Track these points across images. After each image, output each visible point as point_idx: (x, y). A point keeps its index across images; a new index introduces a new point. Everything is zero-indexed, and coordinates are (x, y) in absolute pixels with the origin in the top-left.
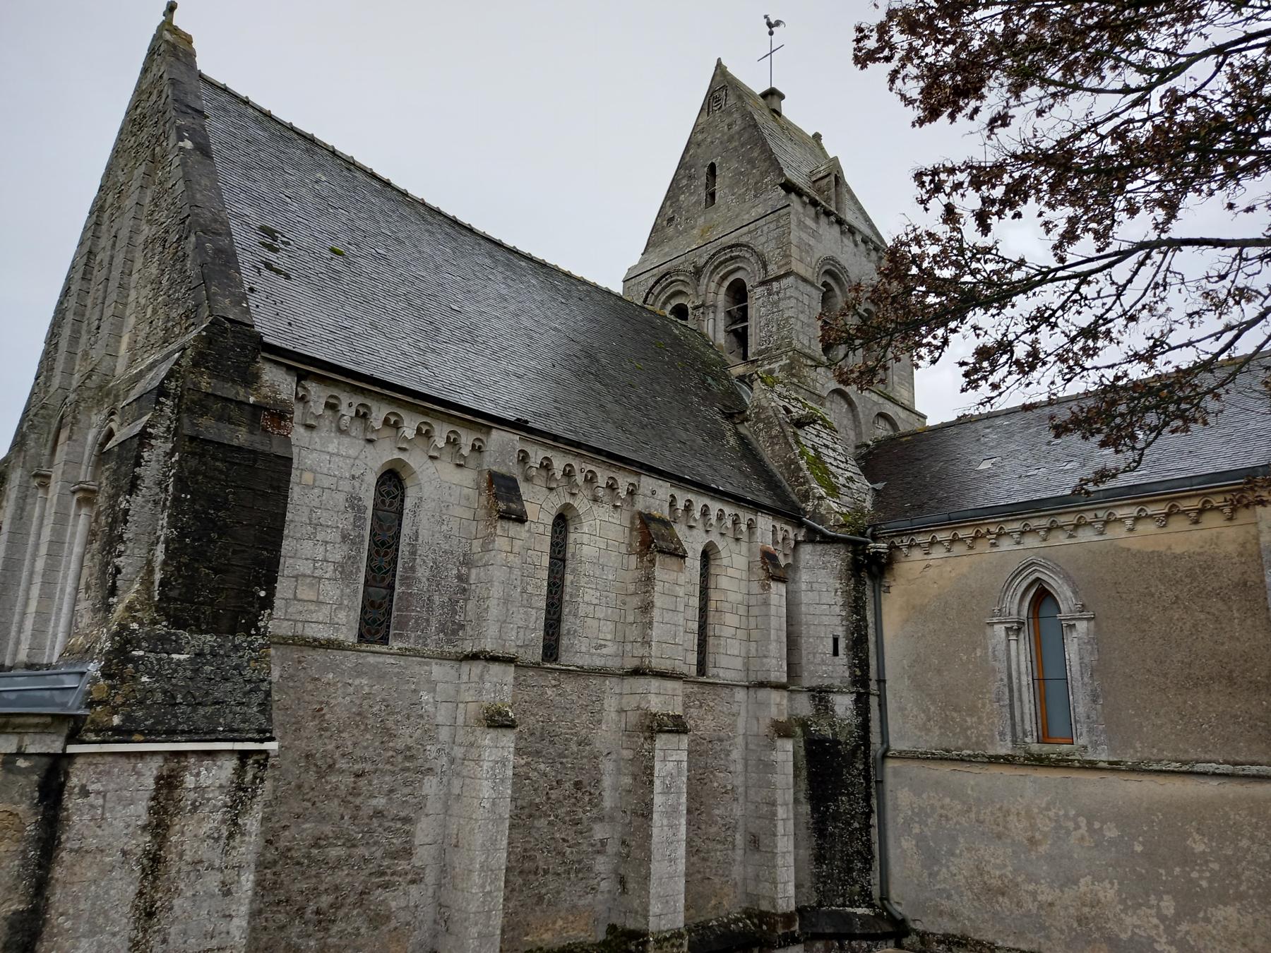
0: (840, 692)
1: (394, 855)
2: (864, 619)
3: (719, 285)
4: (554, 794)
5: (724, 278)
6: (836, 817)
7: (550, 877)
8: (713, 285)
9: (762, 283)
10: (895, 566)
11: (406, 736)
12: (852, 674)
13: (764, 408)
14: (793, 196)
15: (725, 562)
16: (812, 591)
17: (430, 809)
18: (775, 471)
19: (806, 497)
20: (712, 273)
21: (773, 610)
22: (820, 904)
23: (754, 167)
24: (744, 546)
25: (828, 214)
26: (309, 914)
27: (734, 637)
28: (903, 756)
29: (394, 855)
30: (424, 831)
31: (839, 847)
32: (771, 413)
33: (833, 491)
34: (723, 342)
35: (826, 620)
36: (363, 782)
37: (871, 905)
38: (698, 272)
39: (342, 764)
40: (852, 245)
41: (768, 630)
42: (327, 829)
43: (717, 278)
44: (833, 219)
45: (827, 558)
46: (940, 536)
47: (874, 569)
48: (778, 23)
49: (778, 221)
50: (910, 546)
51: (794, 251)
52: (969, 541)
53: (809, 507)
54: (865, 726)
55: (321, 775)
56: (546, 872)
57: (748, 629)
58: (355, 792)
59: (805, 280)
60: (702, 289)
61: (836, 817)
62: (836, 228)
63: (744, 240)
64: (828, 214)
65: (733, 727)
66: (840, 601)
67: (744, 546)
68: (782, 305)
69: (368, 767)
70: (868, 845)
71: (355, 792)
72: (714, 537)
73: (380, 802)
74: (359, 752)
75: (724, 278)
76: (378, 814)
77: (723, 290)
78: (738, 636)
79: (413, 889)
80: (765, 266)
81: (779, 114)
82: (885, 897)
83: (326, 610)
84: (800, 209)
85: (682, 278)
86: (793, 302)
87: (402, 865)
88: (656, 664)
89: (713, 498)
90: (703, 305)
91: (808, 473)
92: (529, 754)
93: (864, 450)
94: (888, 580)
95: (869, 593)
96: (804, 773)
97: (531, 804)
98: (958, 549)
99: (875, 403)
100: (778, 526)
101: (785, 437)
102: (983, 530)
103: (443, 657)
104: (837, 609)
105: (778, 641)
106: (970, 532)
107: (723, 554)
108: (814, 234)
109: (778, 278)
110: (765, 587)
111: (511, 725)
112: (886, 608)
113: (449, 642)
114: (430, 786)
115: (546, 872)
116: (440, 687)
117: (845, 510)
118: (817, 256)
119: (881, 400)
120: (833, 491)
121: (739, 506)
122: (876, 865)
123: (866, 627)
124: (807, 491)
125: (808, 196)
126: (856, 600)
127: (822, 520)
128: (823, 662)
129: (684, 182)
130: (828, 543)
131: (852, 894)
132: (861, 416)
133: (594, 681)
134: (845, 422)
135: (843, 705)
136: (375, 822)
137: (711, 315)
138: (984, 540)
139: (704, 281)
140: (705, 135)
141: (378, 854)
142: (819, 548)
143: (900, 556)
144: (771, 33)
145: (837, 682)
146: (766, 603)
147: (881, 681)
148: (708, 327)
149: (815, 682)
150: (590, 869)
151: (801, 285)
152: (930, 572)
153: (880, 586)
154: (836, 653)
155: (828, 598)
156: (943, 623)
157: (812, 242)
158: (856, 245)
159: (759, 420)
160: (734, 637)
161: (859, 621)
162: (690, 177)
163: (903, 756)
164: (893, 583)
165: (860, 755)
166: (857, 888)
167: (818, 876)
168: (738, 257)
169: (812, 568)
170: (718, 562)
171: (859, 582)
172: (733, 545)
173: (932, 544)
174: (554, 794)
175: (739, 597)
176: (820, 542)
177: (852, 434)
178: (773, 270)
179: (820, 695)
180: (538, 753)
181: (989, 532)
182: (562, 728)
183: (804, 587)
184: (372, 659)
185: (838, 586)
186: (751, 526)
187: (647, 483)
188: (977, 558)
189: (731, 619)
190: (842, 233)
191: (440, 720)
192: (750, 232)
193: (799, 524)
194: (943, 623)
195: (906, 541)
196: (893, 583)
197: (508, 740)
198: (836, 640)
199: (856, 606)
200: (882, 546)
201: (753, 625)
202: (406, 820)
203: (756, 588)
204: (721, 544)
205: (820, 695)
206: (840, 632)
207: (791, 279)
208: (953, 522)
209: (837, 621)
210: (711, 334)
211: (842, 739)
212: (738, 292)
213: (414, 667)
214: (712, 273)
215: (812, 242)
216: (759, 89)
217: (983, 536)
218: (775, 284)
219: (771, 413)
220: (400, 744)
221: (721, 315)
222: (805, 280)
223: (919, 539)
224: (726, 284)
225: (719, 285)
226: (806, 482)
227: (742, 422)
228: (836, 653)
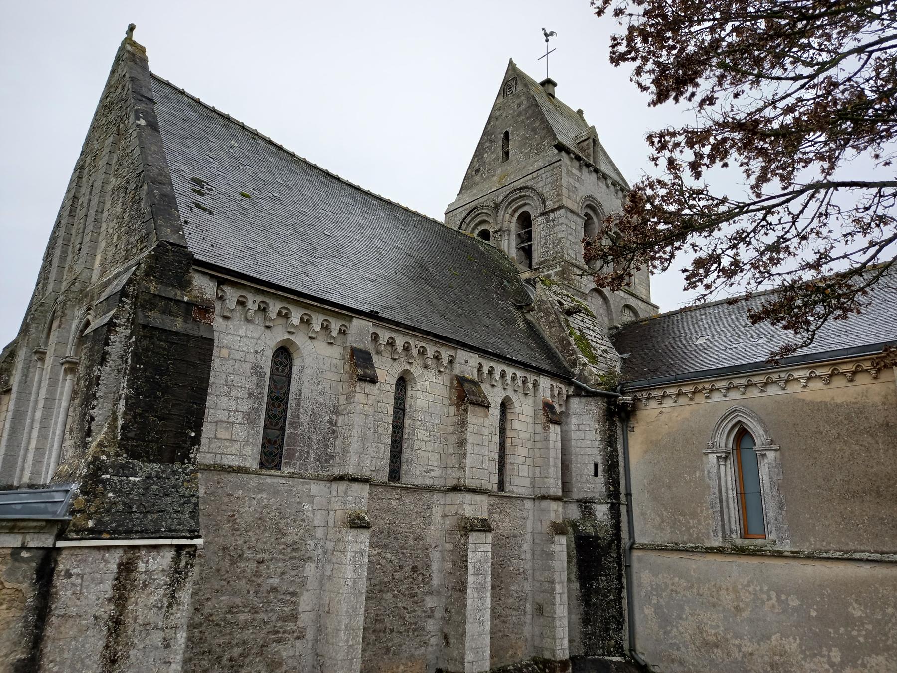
0: (599, 502)
1: (284, 619)
2: (616, 450)
3: (512, 215)
4: (397, 576)
5: (515, 211)
6: (597, 591)
7: (394, 634)
8: (507, 216)
9: (542, 214)
10: (638, 413)
11: (293, 535)
12: (608, 489)
13: (543, 302)
14: (563, 153)
15: (517, 410)
16: (579, 430)
17: (310, 586)
18: (552, 345)
19: (574, 364)
20: (507, 207)
21: (551, 444)
22: (586, 654)
23: (536, 134)
24: (531, 399)
25: (588, 165)
26: (225, 661)
27: (524, 463)
28: (644, 548)
29: (284, 619)
30: (306, 602)
31: (599, 613)
32: (549, 305)
33: (593, 359)
34: (515, 255)
35: (589, 451)
36: (263, 567)
37: (623, 655)
38: (497, 207)
39: (248, 554)
40: (605, 187)
41: (548, 459)
42: (238, 600)
43: (510, 211)
44: (591, 169)
45: (589, 407)
46: (669, 391)
47: (623, 415)
48: (552, 34)
49: (553, 171)
50: (648, 399)
51: (564, 192)
52: (690, 395)
53: (576, 371)
54: (617, 527)
55: (233, 562)
56: (392, 631)
57: (534, 458)
58: (257, 574)
59: (572, 212)
60: (500, 219)
61: (597, 591)
62: (594, 176)
63: (529, 184)
64: (588, 165)
65: (524, 527)
66: (599, 437)
67: (531, 399)
68: (556, 229)
69: (266, 556)
70: (620, 612)
71: (257, 574)
72: (510, 393)
73: (275, 581)
74: (260, 546)
75: (515, 211)
76: (274, 589)
77: (515, 219)
78: (527, 463)
79: (298, 643)
80: (544, 202)
81: (553, 97)
82: (632, 649)
83: (237, 446)
84: (568, 162)
85: (485, 211)
86: (563, 228)
87: (290, 626)
88: (469, 483)
89: (508, 365)
90: (500, 230)
91: (575, 347)
92: (379, 547)
93: (615, 331)
94: (632, 423)
95: (619, 432)
96: (574, 560)
97: (381, 582)
98: (682, 400)
99: (622, 298)
100: (555, 385)
101: (559, 322)
102: (700, 387)
103: (318, 479)
104: (597, 443)
105: (555, 466)
106: (691, 388)
107: (516, 405)
108: (578, 180)
109: (553, 211)
110: (546, 428)
111: (367, 527)
112: (631, 442)
113: (323, 468)
114: (310, 570)
115: (392, 631)
116: (317, 499)
117: (601, 373)
118: (580, 195)
119: (627, 296)
120: (593, 359)
121: (527, 371)
122: (626, 625)
123: (618, 456)
124: (575, 360)
125: (574, 153)
126: (610, 436)
127: (586, 380)
128: (587, 481)
129: (487, 144)
130: (590, 396)
131: (609, 646)
132: (612, 306)
133: (426, 495)
134: (601, 311)
135: (602, 511)
136: (272, 596)
137: (507, 237)
138: (701, 394)
139: (501, 213)
140: (501, 112)
141: (274, 618)
142: (584, 400)
143: (641, 406)
144: (547, 41)
145: (597, 496)
146: (547, 439)
147: (629, 495)
148: (504, 245)
149: (581, 496)
150: (423, 629)
151: (569, 215)
152: (662, 417)
153: (627, 427)
154: (596, 475)
155: (591, 435)
156: (672, 453)
157: (577, 185)
158: (608, 187)
159: (540, 310)
160: (524, 463)
161: (612, 451)
162: (491, 141)
163: (644, 548)
164: (636, 425)
165: (614, 547)
166: (613, 642)
167: (585, 634)
168: (525, 196)
169: (579, 415)
170: (512, 410)
171: (613, 424)
172: (522, 398)
173: (664, 397)
174: (397, 576)
175: (528, 435)
176: (584, 396)
177: (606, 319)
178: (550, 205)
179: (585, 504)
180: (386, 546)
181: (704, 388)
182: (403, 528)
183: (573, 427)
184: (269, 480)
185: (597, 427)
186: (535, 385)
187: (462, 355)
188: (695, 407)
189: (522, 451)
190: (598, 179)
191: (316, 523)
192: (533, 179)
193: (570, 383)
194: (672, 453)
195: (645, 394)
196: (636, 425)
197: (365, 537)
198: (596, 465)
199: (610, 441)
200: (628, 398)
201: (537, 455)
202: (293, 594)
203: (539, 428)
204: (514, 398)
205: (585, 504)
206: (599, 459)
207: (562, 211)
208: (679, 381)
209: (597, 451)
210: (506, 250)
211: (601, 536)
212: (525, 221)
213: (300, 486)
214: (507, 207)
215: (577, 185)
216: (539, 79)
217: (700, 391)
218: (551, 215)
219: (549, 305)
220: (289, 540)
221: (513, 237)
222: (572, 212)
223: (655, 394)
224: (517, 215)
225: (512, 215)
226: (574, 353)
227: (529, 312)
228: (596, 475)
